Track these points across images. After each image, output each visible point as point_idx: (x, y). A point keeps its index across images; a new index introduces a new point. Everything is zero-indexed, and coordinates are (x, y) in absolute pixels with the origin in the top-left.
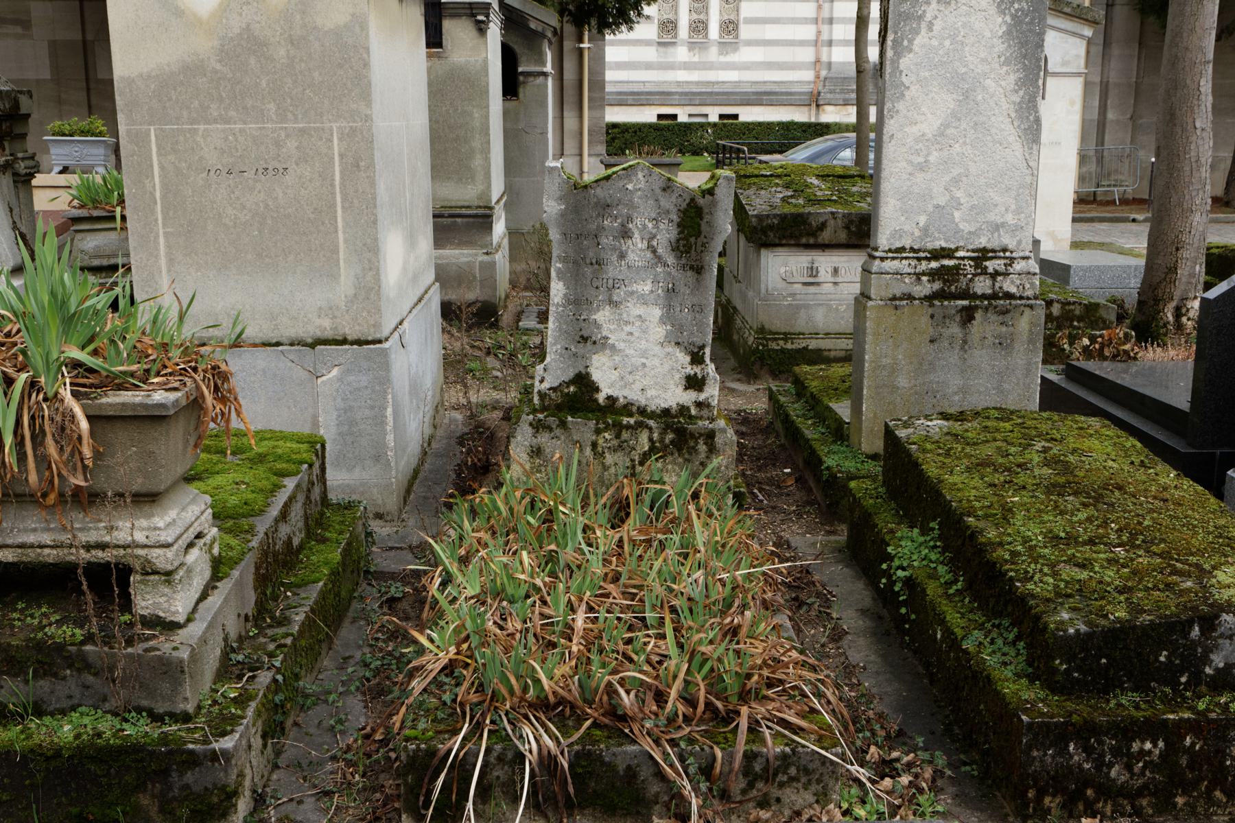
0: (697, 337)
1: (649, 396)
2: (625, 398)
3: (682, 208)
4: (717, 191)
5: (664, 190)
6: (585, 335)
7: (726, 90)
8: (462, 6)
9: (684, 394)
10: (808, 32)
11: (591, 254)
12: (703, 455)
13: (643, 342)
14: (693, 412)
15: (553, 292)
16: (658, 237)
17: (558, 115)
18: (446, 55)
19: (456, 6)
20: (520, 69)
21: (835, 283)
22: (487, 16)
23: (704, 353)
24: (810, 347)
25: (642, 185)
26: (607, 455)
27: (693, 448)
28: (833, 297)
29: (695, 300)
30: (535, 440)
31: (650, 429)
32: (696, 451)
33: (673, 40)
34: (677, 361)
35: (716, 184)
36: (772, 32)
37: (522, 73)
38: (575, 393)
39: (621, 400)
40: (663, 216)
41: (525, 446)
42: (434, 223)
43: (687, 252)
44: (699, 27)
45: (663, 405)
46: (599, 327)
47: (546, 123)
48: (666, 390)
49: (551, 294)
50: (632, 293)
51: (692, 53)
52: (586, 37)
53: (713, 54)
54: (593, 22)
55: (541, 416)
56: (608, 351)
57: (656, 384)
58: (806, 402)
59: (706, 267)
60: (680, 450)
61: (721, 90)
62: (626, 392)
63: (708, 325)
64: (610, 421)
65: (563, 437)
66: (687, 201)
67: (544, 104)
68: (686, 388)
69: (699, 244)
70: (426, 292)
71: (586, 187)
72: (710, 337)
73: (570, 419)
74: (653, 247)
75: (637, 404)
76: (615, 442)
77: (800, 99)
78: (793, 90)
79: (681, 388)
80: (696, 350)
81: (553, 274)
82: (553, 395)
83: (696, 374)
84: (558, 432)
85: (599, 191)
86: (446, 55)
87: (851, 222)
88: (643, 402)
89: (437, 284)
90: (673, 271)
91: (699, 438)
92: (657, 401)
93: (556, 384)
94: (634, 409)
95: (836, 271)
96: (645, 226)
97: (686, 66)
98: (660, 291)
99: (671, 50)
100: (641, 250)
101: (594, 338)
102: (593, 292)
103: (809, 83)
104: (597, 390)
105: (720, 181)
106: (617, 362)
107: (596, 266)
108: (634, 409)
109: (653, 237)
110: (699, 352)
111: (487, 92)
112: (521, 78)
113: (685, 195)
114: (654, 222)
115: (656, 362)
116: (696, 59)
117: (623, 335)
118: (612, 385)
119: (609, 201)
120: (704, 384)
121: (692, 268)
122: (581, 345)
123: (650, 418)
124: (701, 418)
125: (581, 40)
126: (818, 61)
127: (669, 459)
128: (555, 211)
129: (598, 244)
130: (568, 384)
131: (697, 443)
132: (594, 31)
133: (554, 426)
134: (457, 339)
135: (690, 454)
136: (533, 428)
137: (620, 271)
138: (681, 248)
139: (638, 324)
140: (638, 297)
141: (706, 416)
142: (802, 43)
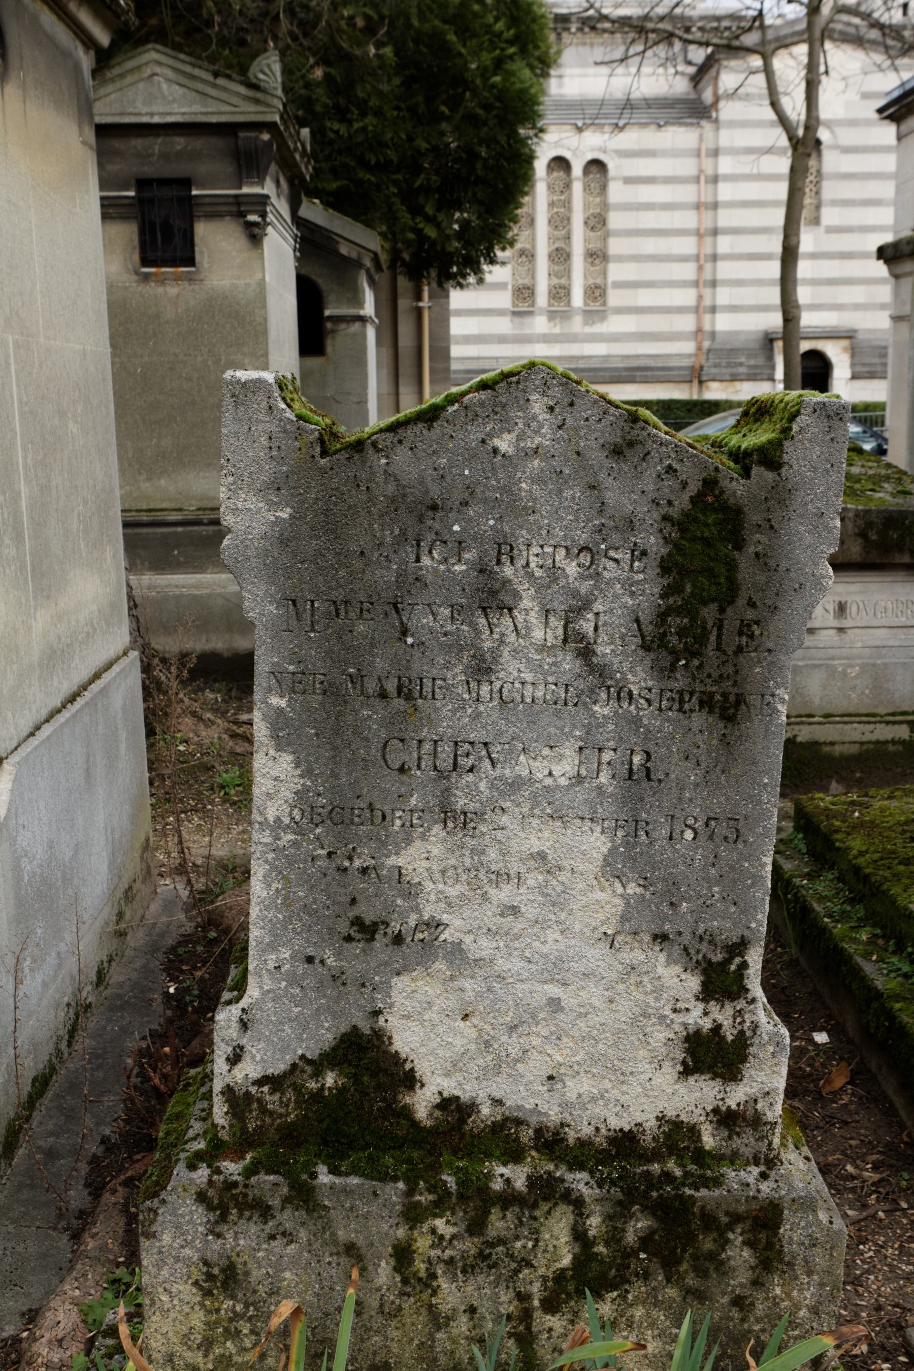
0: (725, 916)
1: (571, 1096)
2: (498, 1102)
3: (674, 512)
4: (792, 453)
5: (617, 452)
6: (368, 919)
7: (592, 366)
8: (222, 200)
9: (681, 1088)
10: (688, 297)
11: (381, 665)
12: (740, 1279)
13: (553, 935)
14: (709, 1141)
15: (261, 787)
16: (598, 607)
17: (387, 388)
18: (202, 276)
19: (214, 200)
20: (327, 313)
21: (841, 630)
22: (263, 215)
23: (744, 965)
24: (799, 739)
25: (544, 438)
26: (443, 1283)
27: (712, 1256)
28: (837, 652)
29: (718, 805)
30: (217, 1245)
31: (578, 1204)
32: (722, 1267)
33: (530, 309)
34: (658, 991)
35: (786, 431)
36: (645, 298)
37: (330, 318)
38: (342, 1091)
39: (485, 1110)
40: (615, 538)
41: (189, 1264)
42: (124, 534)
43: (692, 654)
44: (560, 293)
45: (615, 1123)
46: (411, 891)
47: (365, 387)
48: (623, 1077)
49: (256, 791)
50: (516, 785)
51: (552, 324)
52: (426, 295)
53: (577, 325)
54: (433, 273)
55: (232, 1168)
56: (440, 965)
57: (594, 1060)
58: (839, 879)
59: (753, 699)
60: (670, 1264)
61: (587, 366)
62: (499, 1087)
63: (757, 879)
64: (450, 1180)
65: (303, 1234)
66: (694, 487)
67: (362, 362)
68: (687, 1072)
69: (731, 624)
70: (97, 676)
71: (359, 446)
72: (760, 922)
73: (324, 1177)
74: (582, 637)
75: (534, 1120)
76: (470, 1246)
77: (679, 376)
78: (671, 364)
79: (670, 1071)
80: (718, 957)
81: (261, 730)
82: (272, 1100)
83: (717, 1028)
84: (287, 1218)
85: (401, 457)
86: (202, 276)
87: (870, 525)
88: (553, 1114)
89: (134, 654)
90: (647, 714)
91: (730, 1227)
92: (598, 1110)
93: (280, 1067)
94: (526, 1135)
95: (842, 609)
96: (554, 572)
97: (546, 339)
98: (604, 778)
99: (527, 320)
100: (543, 648)
101: (395, 926)
102: (391, 783)
103: (689, 356)
104: (410, 1080)
105: (802, 420)
106: (469, 995)
107: (399, 703)
108: (526, 1135)
109: (583, 605)
110: (728, 961)
111: (265, 332)
112: (329, 325)
113: (685, 470)
114: (585, 558)
115: (594, 994)
116: (557, 330)
117: (489, 916)
118: (454, 1067)
119: (435, 491)
120: (744, 1059)
121: (706, 703)
122: (357, 948)
123: (576, 1165)
124: (733, 1158)
125: (419, 297)
126: (699, 330)
127: (637, 1289)
128: (259, 529)
129: (404, 632)
130: (318, 1066)
131: (724, 1243)
132: (434, 285)
133: (276, 1202)
134: (209, 724)
135: (702, 1273)
136: (210, 1208)
137: (477, 716)
138: (674, 640)
139: (534, 879)
140: (535, 796)
141: (748, 1152)
142: (680, 310)
